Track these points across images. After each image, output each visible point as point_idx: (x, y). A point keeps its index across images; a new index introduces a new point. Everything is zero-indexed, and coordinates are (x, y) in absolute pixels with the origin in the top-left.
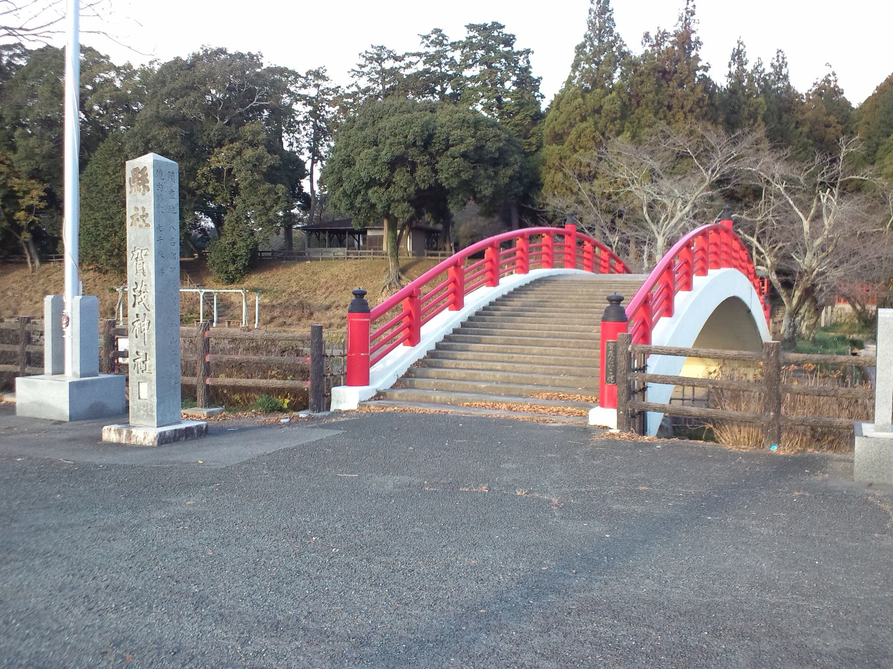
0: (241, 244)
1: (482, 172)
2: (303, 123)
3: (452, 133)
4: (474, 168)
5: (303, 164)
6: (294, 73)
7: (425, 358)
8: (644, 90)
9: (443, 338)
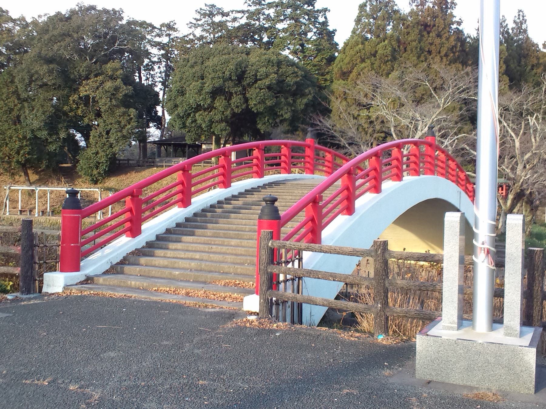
0: (101, 154)
1: (283, 100)
2: (158, 62)
3: (260, 70)
4: (277, 97)
5: (157, 94)
6: (151, 25)
7: (143, 247)
8: (410, 39)
9: (164, 231)
